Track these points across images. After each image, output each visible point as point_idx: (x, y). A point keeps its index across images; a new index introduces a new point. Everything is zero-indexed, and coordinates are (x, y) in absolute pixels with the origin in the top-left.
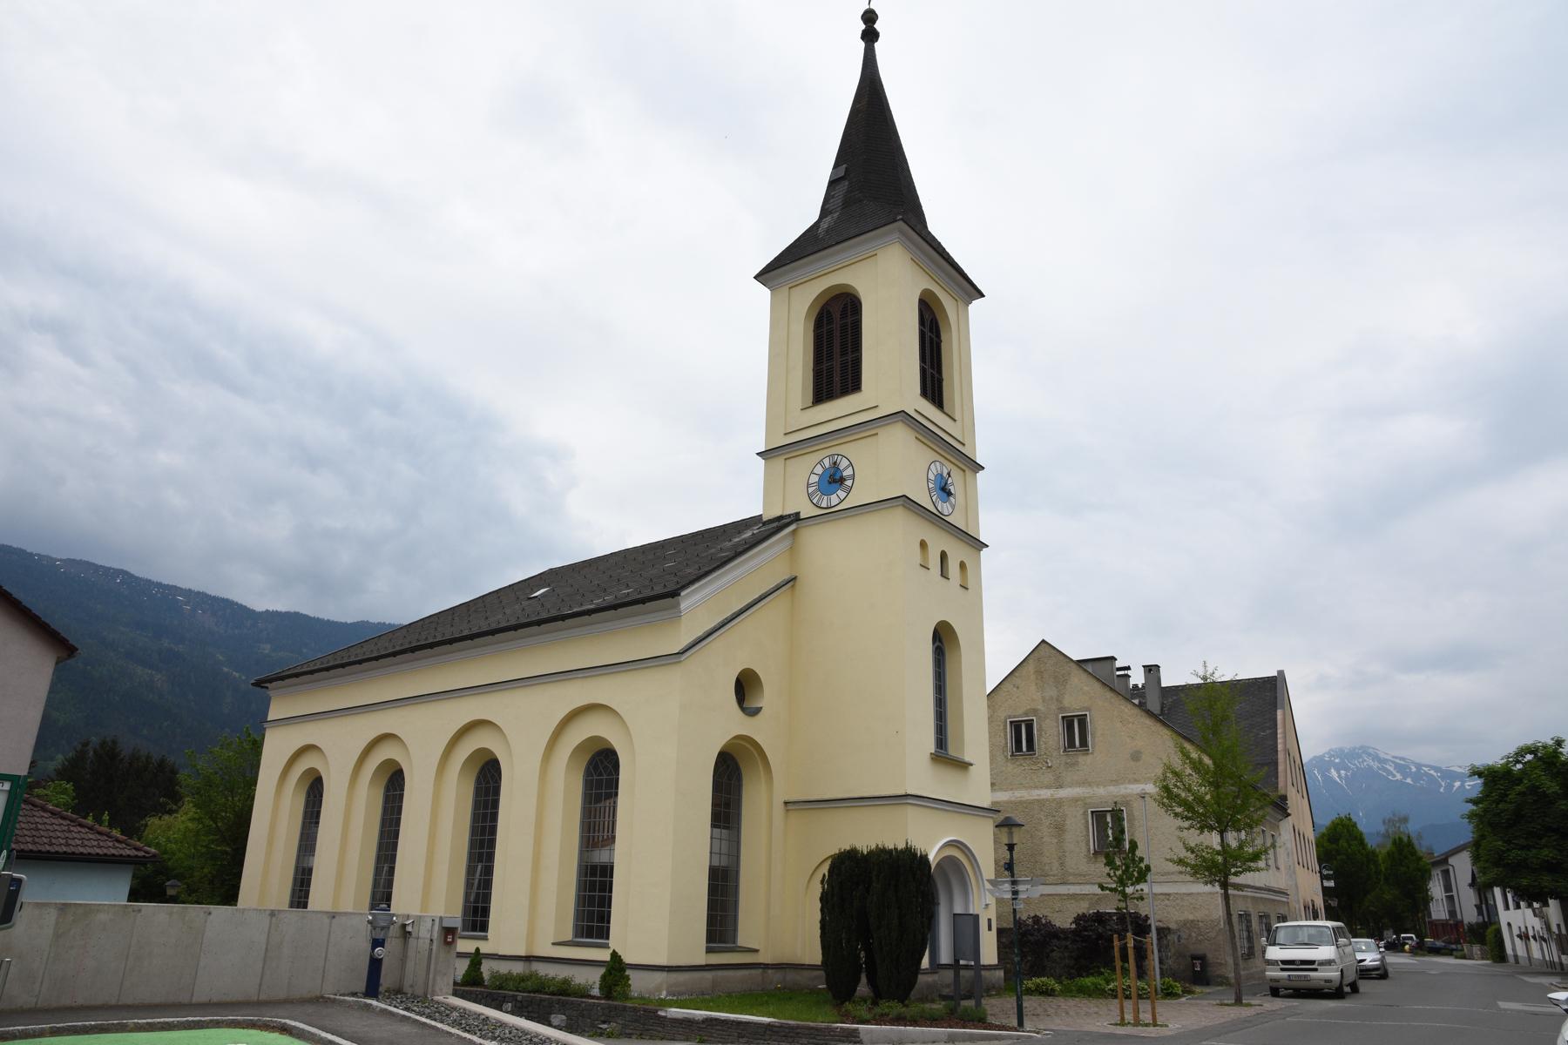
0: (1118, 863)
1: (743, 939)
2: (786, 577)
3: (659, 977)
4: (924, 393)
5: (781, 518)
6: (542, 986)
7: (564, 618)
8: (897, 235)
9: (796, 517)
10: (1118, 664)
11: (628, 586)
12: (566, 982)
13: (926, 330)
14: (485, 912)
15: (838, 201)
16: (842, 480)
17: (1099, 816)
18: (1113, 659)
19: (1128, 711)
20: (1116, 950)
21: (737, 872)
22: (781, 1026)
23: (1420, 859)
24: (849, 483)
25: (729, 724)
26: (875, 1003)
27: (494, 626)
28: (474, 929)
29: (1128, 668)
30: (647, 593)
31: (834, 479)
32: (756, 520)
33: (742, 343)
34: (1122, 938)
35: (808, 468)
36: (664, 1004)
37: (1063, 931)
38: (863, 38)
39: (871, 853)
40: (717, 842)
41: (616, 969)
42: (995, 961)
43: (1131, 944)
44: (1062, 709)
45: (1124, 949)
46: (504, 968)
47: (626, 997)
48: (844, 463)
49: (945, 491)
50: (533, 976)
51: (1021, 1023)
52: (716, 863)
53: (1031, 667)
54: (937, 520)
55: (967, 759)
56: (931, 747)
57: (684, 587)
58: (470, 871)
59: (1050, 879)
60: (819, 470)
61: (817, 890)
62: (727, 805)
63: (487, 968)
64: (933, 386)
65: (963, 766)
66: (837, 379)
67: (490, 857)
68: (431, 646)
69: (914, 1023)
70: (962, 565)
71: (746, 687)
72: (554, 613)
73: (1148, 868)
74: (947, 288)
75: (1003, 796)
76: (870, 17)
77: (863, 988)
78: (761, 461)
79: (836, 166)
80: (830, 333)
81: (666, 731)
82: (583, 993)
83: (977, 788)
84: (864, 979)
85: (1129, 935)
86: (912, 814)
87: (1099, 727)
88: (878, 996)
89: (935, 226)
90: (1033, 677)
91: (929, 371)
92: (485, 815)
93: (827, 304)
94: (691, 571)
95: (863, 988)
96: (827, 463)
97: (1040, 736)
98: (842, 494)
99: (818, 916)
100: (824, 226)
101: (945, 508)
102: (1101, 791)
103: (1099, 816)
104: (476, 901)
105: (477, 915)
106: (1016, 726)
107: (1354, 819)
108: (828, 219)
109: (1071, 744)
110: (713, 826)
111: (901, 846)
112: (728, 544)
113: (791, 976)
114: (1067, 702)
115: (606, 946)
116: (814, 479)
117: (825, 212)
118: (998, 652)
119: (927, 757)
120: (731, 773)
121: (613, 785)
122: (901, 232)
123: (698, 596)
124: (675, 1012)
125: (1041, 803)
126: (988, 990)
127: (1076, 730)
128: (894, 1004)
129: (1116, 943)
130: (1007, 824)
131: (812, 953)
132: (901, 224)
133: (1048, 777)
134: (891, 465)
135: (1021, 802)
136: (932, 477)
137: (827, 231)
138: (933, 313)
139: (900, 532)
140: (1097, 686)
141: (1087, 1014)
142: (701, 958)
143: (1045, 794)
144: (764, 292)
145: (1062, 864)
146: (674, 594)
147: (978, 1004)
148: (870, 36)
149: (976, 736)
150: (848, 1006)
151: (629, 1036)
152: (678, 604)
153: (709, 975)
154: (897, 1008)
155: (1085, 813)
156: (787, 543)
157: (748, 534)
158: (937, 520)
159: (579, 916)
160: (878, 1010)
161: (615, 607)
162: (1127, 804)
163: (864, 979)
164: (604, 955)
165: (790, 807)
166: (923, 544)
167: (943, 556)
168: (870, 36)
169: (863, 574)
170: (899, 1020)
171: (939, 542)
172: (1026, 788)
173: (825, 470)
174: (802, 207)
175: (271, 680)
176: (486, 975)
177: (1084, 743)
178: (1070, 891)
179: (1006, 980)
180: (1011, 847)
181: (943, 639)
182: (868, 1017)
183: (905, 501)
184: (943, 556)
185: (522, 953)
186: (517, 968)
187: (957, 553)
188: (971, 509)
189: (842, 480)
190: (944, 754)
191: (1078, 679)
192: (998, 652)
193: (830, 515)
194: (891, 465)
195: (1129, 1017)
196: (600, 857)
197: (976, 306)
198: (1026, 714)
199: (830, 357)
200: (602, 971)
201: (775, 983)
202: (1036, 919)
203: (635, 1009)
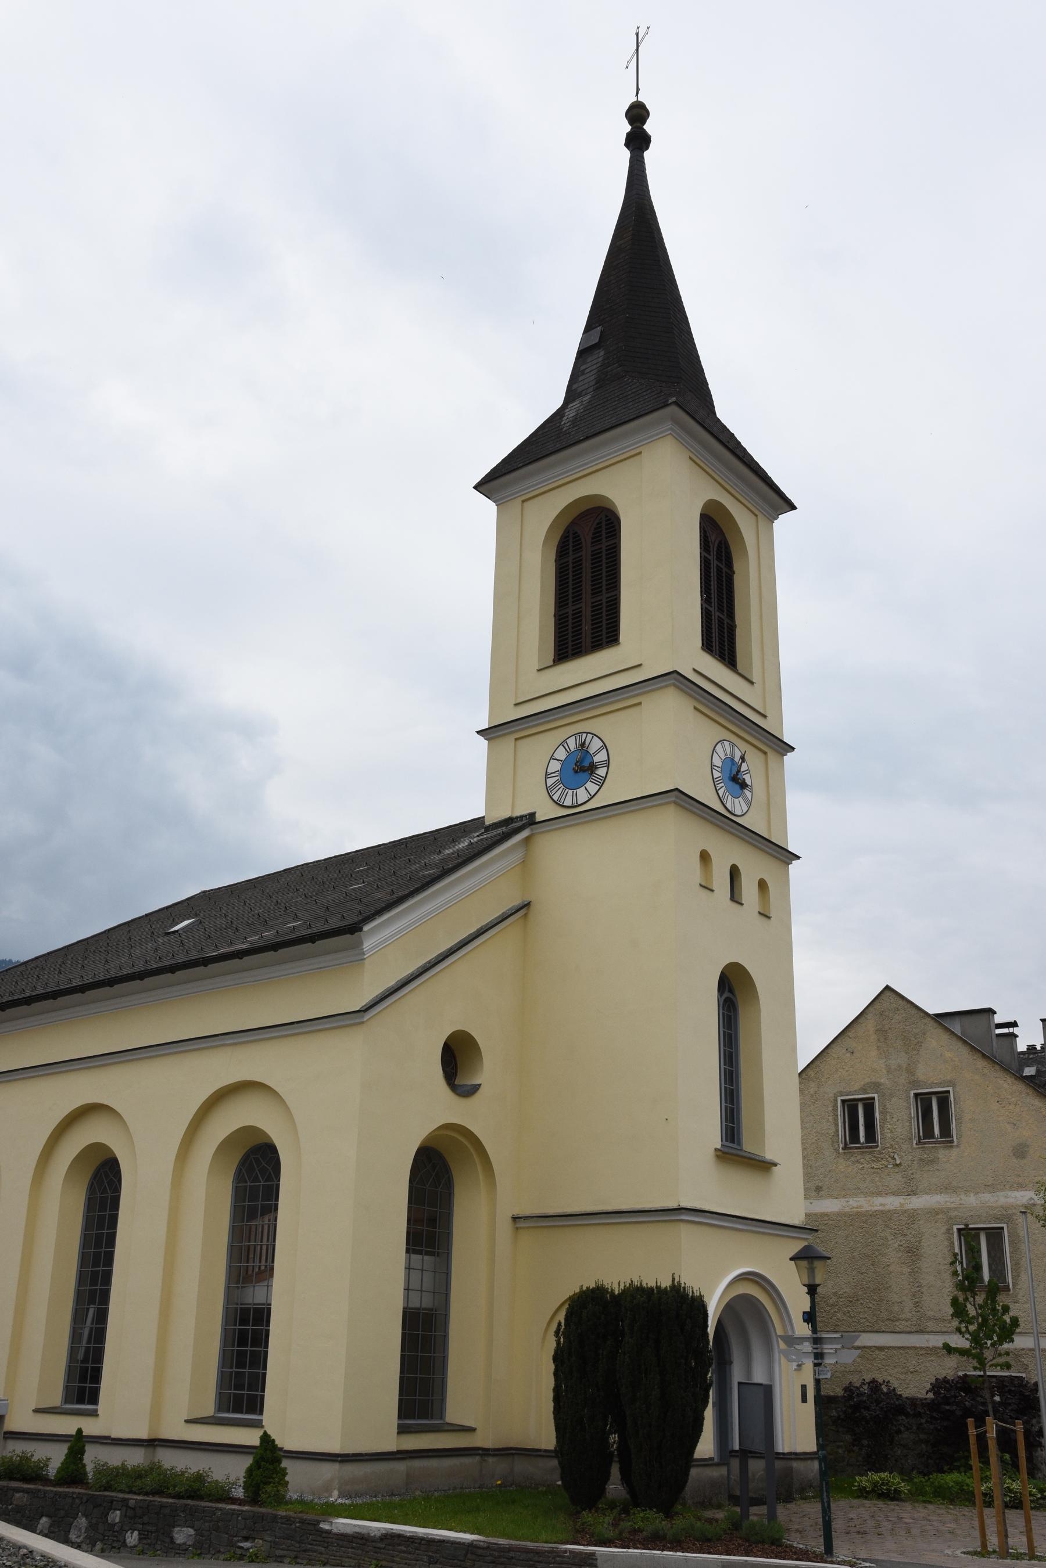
0: (972, 1311)
1: (453, 1414)
2: (517, 903)
3: (328, 1471)
4: (708, 646)
5: (510, 820)
6: (163, 1484)
7: (206, 962)
8: (669, 425)
9: (530, 820)
10: (998, 1019)
11: (296, 918)
12: (199, 1478)
13: (712, 557)
14: (96, 1375)
15: (589, 379)
16: (592, 768)
17: (969, 1235)
18: (990, 1012)
19: (1008, 1085)
20: (972, 1440)
21: (446, 1316)
22: (489, 1547)
24: (602, 772)
25: (433, 1108)
26: (625, 1510)
27: (114, 973)
28: (80, 1401)
29: (1014, 1024)
30: (319, 927)
31: (582, 767)
32: (477, 823)
33: (459, 573)
34: (980, 1422)
35: (546, 752)
36: (334, 1510)
37: (913, 1401)
38: (627, 145)
39: (625, 1292)
40: (416, 1276)
41: (268, 1458)
42: (812, 1447)
43: (992, 1434)
44: (915, 1083)
45: (982, 1438)
46: (114, 1457)
47: (280, 1500)
48: (596, 744)
49: (737, 781)
50: (154, 1468)
51: (829, 1549)
52: (415, 1303)
53: (870, 1024)
54: (726, 823)
55: (769, 1156)
56: (716, 1140)
57: (368, 919)
58: (78, 1317)
59: (901, 1325)
60: (561, 754)
61: (551, 1344)
62: (432, 1221)
63: (93, 1457)
64: (721, 634)
65: (764, 1166)
66: (586, 627)
67: (104, 1297)
68: (28, 1001)
69: (677, 1545)
70: (762, 885)
71: (457, 1058)
72: (194, 955)
73: (1015, 1322)
74: (742, 496)
75: (830, 1206)
76: (637, 114)
77: (615, 1487)
78: (483, 743)
79: (588, 329)
80: (578, 563)
81: (345, 1120)
82: (222, 1495)
83: (786, 1198)
84: (615, 1470)
85: (989, 1420)
86: (687, 1235)
87: (966, 1108)
88: (636, 1499)
89: (726, 411)
90: (873, 1037)
91: (716, 614)
92: (99, 1237)
93: (573, 523)
94: (382, 896)
95: (615, 1487)
96: (572, 744)
97: (884, 1120)
98: (592, 787)
99: (551, 1382)
100: (570, 413)
101: (738, 805)
102: (972, 1200)
103: (969, 1235)
104: (85, 1360)
105: (84, 1382)
106: (850, 1107)
107: (941, 1377)
108: (576, 404)
109: (928, 1132)
110: (408, 1251)
111: (666, 1283)
112: (437, 857)
113: (521, 1466)
114: (921, 1073)
115: (258, 1424)
116: (555, 766)
117: (572, 393)
118: (821, 998)
119: (710, 1153)
120: (436, 1176)
121: (272, 1193)
122: (676, 421)
123: (387, 932)
124: (344, 1524)
125: (887, 1216)
126: (802, 1490)
127: (935, 1113)
128: (651, 1514)
129: (972, 1431)
130: (806, 1257)
131: (543, 1434)
132: (674, 409)
133: (896, 1180)
134: (660, 748)
135: (858, 1214)
136: (717, 762)
137: (575, 421)
138: (721, 532)
139: (672, 838)
140: (964, 1051)
141: (938, 1534)
142: (390, 1442)
143: (892, 1203)
144: (488, 508)
145: (917, 1304)
146: (354, 929)
147: (772, 1516)
148: (638, 141)
149: (781, 1125)
150: (587, 1517)
151: (280, 1559)
152: (361, 943)
153: (401, 1467)
154: (651, 1520)
155: (949, 1231)
156: (516, 857)
157: (464, 844)
158: (726, 823)
159: (224, 1380)
160: (626, 1525)
161: (275, 947)
163: (615, 1470)
164: (251, 1437)
165: (521, 1224)
166: (705, 857)
167: (734, 873)
168: (638, 141)
169: (621, 895)
170: (657, 1541)
171: (727, 853)
172: (865, 1194)
173: (570, 754)
174: (536, 383)
176: (90, 1468)
177: (946, 1131)
178: (916, 1353)
180: (812, 1289)
181: (734, 989)
182: (611, 1534)
183: (679, 798)
184: (734, 873)
185: (144, 1435)
186: (135, 1458)
187: (754, 867)
188: (775, 806)
189: (592, 768)
190: (736, 1149)
191: (936, 1041)
192: (821, 998)
193: (576, 817)
194: (660, 748)
195: (993, 1541)
196: (254, 1296)
197: (783, 523)
198: (864, 1090)
199: (578, 597)
200: (248, 1461)
201: (491, 1481)
202: (874, 1385)
203: (288, 1520)
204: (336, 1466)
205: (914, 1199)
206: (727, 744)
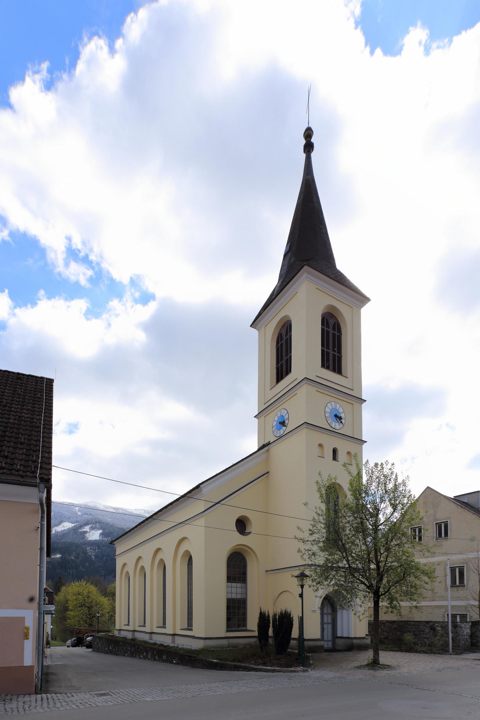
4: (325, 364)
9: (269, 444)
23: (91, 584)
25: (236, 539)
44: (435, 520)
71: (242, 525)
76: (308, 134)
102: (454, 558)
109: (440, 535)
136: (328, 410)
142: (223, 634)
148: (309, 147)
162: (467, 563)
165: (268, 573)
166: (320, 445)
167: (335, 451)
168: (309, 147)
171: (330, 442)
175: (115, 540)
179: (260, 642)
184: (335, 451)
185: (172, 633)
187: (343, 447)
204: (202, 641)
205: (433, 558)
206: (333, 403)
